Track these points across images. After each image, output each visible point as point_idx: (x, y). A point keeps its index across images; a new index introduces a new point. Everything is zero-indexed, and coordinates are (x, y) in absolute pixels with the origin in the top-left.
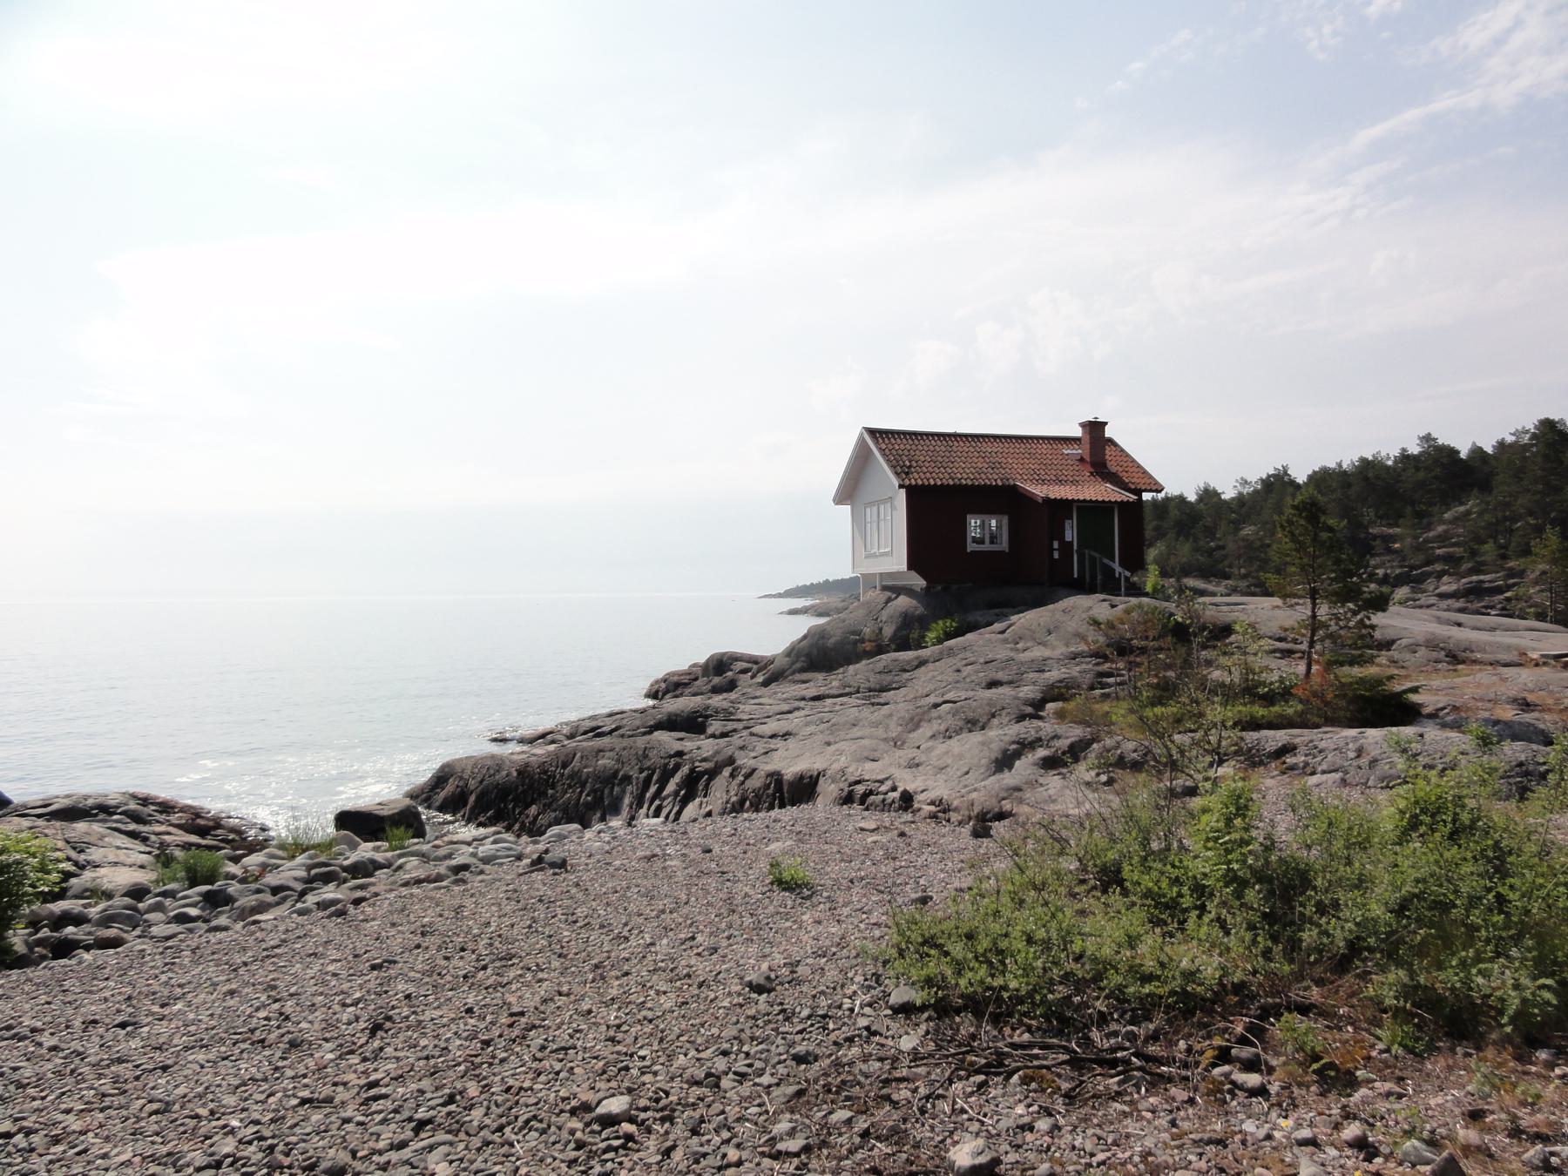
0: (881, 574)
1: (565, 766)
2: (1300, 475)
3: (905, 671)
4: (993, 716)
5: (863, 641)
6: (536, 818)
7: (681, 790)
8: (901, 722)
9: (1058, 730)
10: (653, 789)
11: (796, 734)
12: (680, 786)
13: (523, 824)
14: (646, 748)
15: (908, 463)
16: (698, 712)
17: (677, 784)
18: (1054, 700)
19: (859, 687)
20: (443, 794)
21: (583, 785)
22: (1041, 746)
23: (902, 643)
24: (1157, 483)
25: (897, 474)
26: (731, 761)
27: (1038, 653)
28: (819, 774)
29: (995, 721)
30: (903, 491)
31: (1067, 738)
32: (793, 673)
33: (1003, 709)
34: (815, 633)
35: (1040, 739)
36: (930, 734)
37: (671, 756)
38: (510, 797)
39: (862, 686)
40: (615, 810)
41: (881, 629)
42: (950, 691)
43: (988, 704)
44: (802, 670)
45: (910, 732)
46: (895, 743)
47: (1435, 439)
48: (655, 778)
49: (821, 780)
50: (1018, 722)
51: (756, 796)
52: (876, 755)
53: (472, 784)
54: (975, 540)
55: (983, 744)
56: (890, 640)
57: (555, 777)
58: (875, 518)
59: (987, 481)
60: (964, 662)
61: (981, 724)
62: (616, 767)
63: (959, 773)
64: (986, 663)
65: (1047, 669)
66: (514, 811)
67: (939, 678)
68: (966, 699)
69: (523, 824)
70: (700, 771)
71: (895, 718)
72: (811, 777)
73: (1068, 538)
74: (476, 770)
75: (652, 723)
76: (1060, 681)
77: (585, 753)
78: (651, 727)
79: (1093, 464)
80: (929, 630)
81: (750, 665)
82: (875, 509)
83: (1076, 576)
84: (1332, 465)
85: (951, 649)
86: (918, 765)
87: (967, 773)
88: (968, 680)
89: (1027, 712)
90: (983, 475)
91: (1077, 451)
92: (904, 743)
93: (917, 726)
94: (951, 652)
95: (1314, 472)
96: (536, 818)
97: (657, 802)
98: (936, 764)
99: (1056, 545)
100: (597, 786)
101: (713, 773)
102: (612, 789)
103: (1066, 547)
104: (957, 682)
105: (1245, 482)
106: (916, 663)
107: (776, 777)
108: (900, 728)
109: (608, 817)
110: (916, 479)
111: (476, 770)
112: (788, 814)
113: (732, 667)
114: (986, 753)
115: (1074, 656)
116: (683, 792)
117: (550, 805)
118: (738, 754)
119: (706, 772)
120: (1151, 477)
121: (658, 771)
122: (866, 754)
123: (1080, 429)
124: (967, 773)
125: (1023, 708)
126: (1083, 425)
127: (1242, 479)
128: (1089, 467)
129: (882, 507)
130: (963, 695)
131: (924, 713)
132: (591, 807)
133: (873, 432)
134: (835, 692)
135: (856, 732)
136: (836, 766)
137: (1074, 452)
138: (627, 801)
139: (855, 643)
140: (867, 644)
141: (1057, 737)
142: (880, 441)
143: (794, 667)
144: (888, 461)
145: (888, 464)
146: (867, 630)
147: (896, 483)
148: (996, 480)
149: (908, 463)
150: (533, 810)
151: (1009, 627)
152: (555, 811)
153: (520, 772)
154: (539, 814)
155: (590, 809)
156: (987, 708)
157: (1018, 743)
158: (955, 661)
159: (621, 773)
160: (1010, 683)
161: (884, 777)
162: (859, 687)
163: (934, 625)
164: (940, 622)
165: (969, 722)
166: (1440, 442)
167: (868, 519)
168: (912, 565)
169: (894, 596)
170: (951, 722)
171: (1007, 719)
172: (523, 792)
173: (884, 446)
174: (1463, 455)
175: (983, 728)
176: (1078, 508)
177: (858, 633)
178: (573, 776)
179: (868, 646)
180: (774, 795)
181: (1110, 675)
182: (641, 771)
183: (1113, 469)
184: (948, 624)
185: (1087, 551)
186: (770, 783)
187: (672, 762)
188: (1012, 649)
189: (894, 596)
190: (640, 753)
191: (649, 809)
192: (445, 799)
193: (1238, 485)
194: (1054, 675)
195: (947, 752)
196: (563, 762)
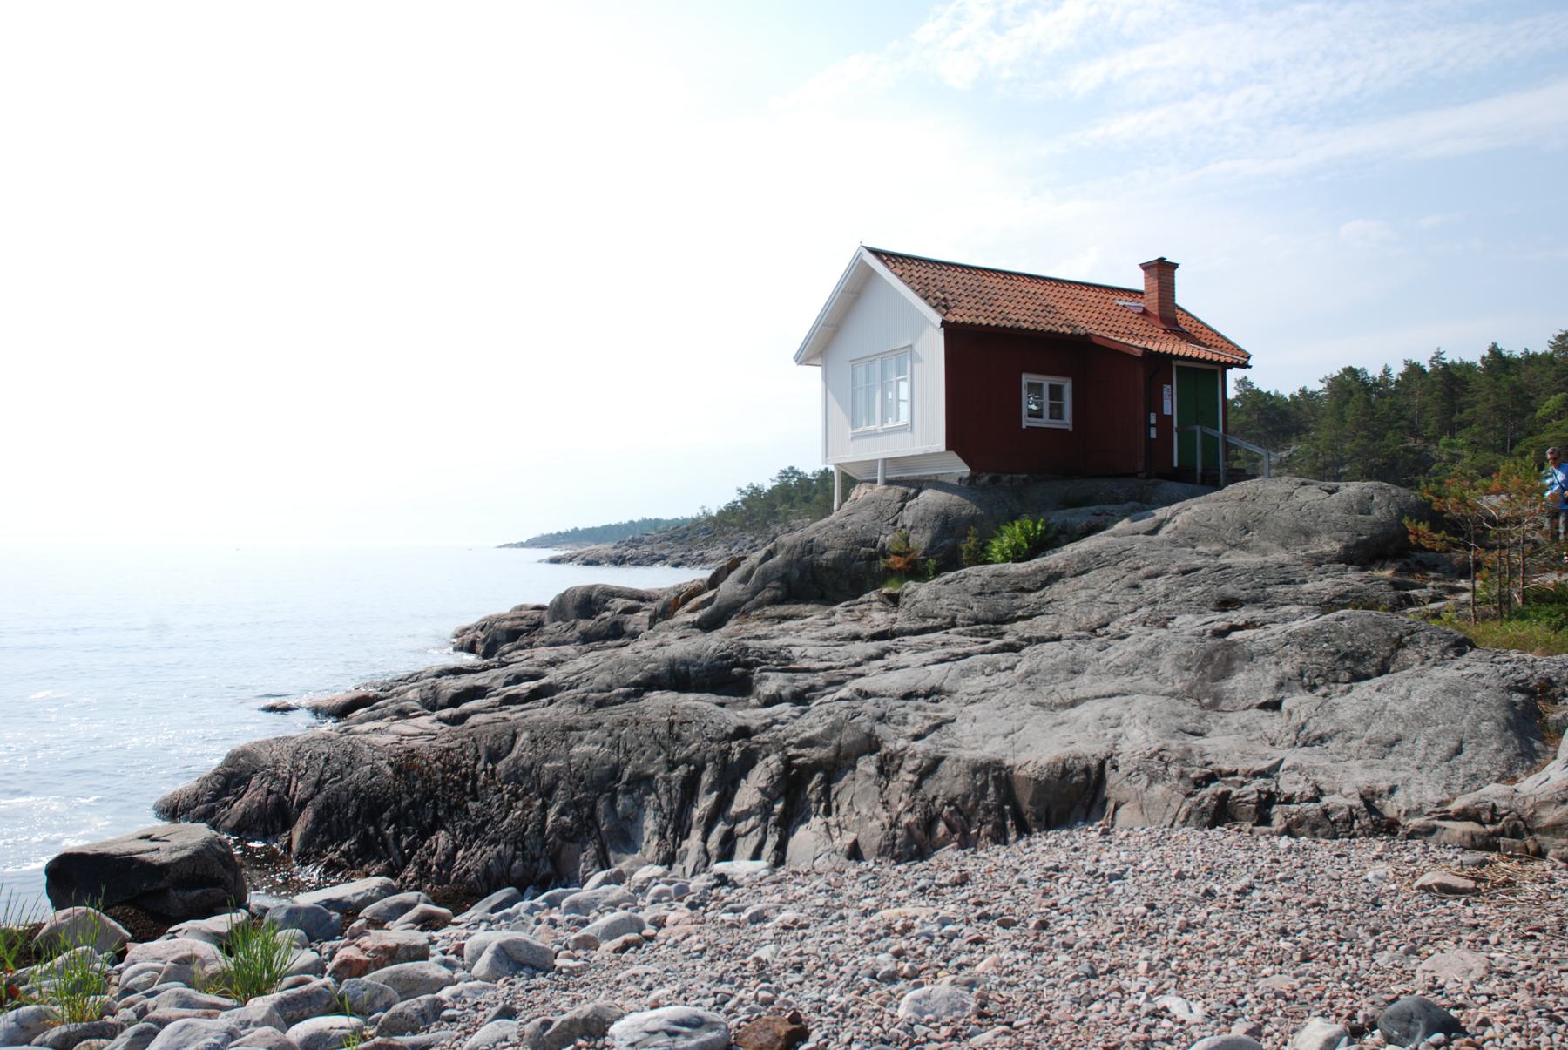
0: (885, 460)
1: (494, 756)
3: (1022, 590)
5: (884, 553)
6: (451, 857)
7: (775, 801)
8: (1184, 662)
10: (705, 803)
12: (769, 796)
13: (423, 864)
14: (671, 724)
16: (729, 656)
17: (763, 791)
20: (239, 807)
21: (548, 793)
26: (871, 744)
28: (1102, 764)
29: (1410, 654)
37: (731, 737)
38: (386, 815)
40: (626, 840)
44: (774, 601)
47: (1251, 383)
48: (706, 778)
49: (1112, 778)
51: (958, 811)
53: (300, 789)
54: (1032, 414)
56: (925, 553)
57: (475, 778)
62: (614, 758)
65: (1298, 580)
66: (397, 840)
69: (423, 864)
70: (805, 765)
72: (1087, 770)
73: (1167, 411)
74: (303, 763)
75: (637, 677)
77: (538, 733)
78: (636, 684)
83: (1176, 464)
91: (1137, 305)
96: (451, 857)
97: (720, 828)
100: (579, 795)
101: (836, 767)
102: (612, 802)
103: (1165, 421)
106: (1040, 578)
107: (996, 775)
109: (612, 855)
111: (303, 763)
112: (1047, 847)
116: (778, 807)
117: (479, 830)
118: (880, 730)
119: (817, 766)
121: (710, 766)
123: (1142, 272)
126: (1146, 267)
128: (1157, 322)
132: (574, 836)
138: (650, 823)
139: (873, 558)
143: (758, 597)
150: (441, 839)
152: (494, 842)
153: (398, 770)
154: (456, 848)
155: (571, 840)
159: (628, 771)
162: (954, 618)
165: (1345, 657)
166: (1255, 386)
168: (953, 442)
169: (912, 491)
172: (412, 805)
174: (1428, 369)
175: (1383, 670)
176: (1178, 368)
178: (516, 775)
179: (896, 562)
180: (1000, 808)
182: (672, 765)
183: (1187, 329)
185: (1198, 428)
186: (985, 786)
187: (736, 749)
189: (912, 491)
190: (662, 731)
191: (705, 840)
192: (244, 815)
196: (489, 749)
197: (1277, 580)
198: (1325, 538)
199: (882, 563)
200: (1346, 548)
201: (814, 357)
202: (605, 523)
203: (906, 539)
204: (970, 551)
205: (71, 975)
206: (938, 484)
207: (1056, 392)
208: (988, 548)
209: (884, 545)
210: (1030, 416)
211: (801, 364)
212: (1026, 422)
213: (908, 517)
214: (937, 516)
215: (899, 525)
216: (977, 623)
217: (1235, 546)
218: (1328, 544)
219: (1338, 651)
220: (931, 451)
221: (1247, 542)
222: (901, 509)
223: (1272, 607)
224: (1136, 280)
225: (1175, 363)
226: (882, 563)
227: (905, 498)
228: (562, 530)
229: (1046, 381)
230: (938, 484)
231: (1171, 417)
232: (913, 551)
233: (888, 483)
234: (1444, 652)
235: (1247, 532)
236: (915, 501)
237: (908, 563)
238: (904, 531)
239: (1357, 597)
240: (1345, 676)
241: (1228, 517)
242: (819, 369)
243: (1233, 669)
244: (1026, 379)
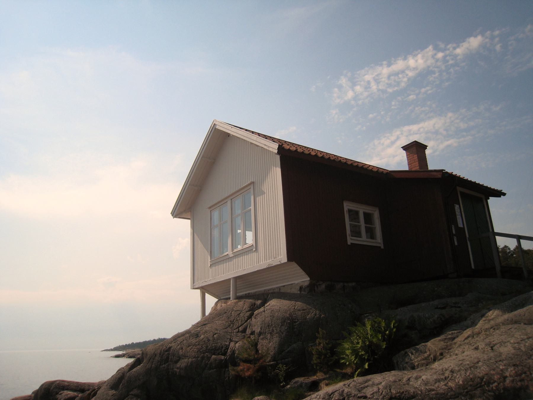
0: (236, 279)
2: (130, 343)
5: (234, 361)
56: (274, 359)
81: (76, 394)
83: (473, 267)
123: (404, 153)
139: (223, 366)
140: (242, 366)
169: (259, 302)
189: (259, 302)
199: (232, 371)
201: (185, 211)
202: (144, 340)
203: (255, 345)
204: (320, 354)
206: (280, 294)
207: (368, 218)
208: (338, 349)
209: (233, 352)
211: (175, 217)
213: (256, 324)
214: (284, 320)
215: (248, 331)
220: (274, 264)
222: (250, 317)
226: (232, 371)
227: (253, 308)
228: (128, 344)
229: (362, 209)
230: (280, 294)
232: (262, 358)
233: (239, 298)
236: (262, 309)
237: (258, 371)
238: (252, 337)
242: (188, 222)
244: (347, 206)
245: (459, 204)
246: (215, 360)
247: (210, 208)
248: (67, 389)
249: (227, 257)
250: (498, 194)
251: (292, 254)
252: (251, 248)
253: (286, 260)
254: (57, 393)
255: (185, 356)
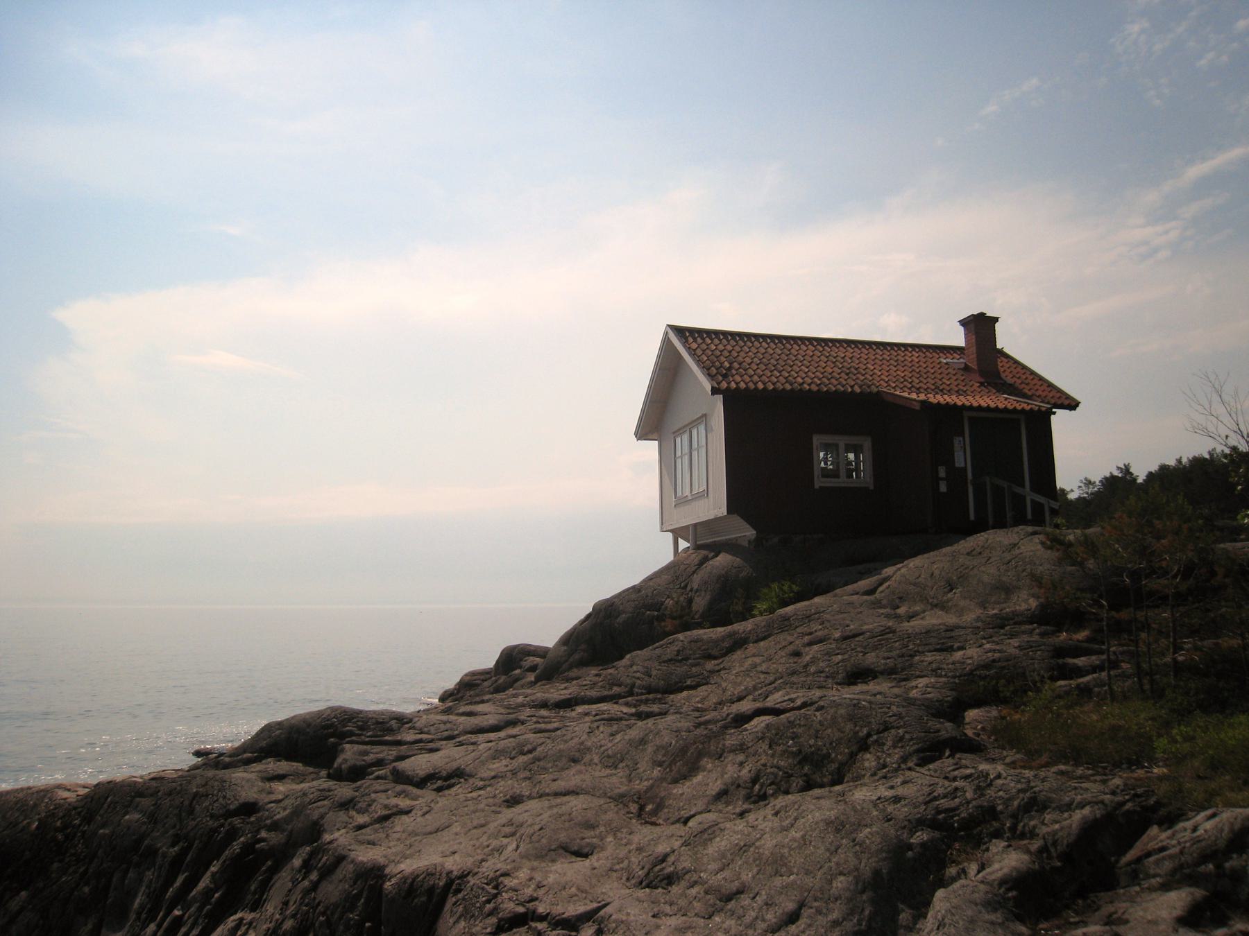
0: (695, 525)
4: (864, 746)
9: (1038, 786)
11: (471, 776)
15: (727, 365)
16: (332, 725)
18: (977, 704)
19: (633, 686)
22: (997, 835)
23: (717, 617)
24: (1068, 397)
25: (711, 376)
27: (933, 619)
29: (869, 760)
30: (719, 399)
31: (1069, 807)
32: (570, 668)
33: (887, 729)
34: (600, 610)
35: (990, 813)
36: (715, 787)
37: (230, 814)
39: (639, 682)
41: (690, 601)
42: (777, 689)
43: (851, 718)
45: (675, 781)
46: (642, 808)
50: (923, 762)
52: (590, 837)
54: (826, 473)
55: (836, 826)
58: (686, 450)
59: (839, 387)
60: (806, 639)
61: (834, 766)
63: (771, 917)
64: (845, 638)
65: (956, 645)
67: (764, 667)
68: (804, 705)
70: (262, 850)
71: (650, 749)
72: (431, 890)
73: (959, 461)
76: (986, 666)
78: (261, 750)
79: (982, 372)
80: (758, 599)
82: (686, 437)
83: (972, 517)
84: (1172, 462)
85: (786, 618)
86: (670, 880)
87: (793, 918)
88: (813, 669)
89: (944, 734)
90: (833, 380)
92: (660, 807)
93: (692, 769)
94: (786, 624)
95: (1163, 468)
98: (714, 880)
99: (942, 472)
103: (957, 476)
104: (794, 673)
105: (1089, 483)
108: (656, 772)
110: (738, 382)
113: (523, 663)
114: (846, 856)
115: (1001, 623)
120: (1059, 391)
122: (563, 837)
123: (962, 329)
124: (793, 918)
125: (933, 724)
126: (964, 323)
127: (1086, 479)
129: (694, 432)
130: (800, 696)
131: (709, 738)
133: (680, 331)
134: (594, 693)
135: (573, 777)
136: (488, 869)
137: (955, 361)
141: (1035, 805)
142: (691, 340)
143: (571, 660)
144: (699, 362)
145: (698, 365)
146: (669, 602)
147: (707, 386)
148: (852, 387)
149: (727, 365)
151: (881, 584)
156: (849, 727)
157: (933, 824)
158: (790, 639)
160: (890, 672)
161: (581, 909)
162: (633, 686)
163: (765, 590)
164: (775, 586)
167: (679, 453)
170: (764, 757)
171: (897, 755)
173: (694, 346)
175: (838, 781)
176: (970, 419)
177: (657, 606)
181: (1077, 651)
183: (1009, 380)
184: (786, 588)
186: (359, 896)
188: (888, 616)
193: (1082, 485)
194: (972, 654)
195: (747, 846)
197: (931, 647)
198: (1024, 594)
200: (1043, 607)
201: (646, 434)
205: (1171, 837)
210: (824, 476)
212: (818, 483)
215: (689, 588)
216: (649, 693)
217: (936, 606)
218: (1026, 601)
219: (800, 751)
221: (948, 601)
223: (905, 680)
224: (957, 338)
225: (966, 414)
231: (965, 469)
234: (904, 759)
235: (951, 590)
239: (1003, 668)
240: (797, 782)
241: (937, 573)
243: (698, 768)
244: (817, 440)
245: (962, 434)
246: (648, 616)
247: (674, 433)
248: (534, 656)
249: (686, 499)
250: (1072, 405)
251: (734, 503)
252: (702, 494)
253: (726, 514)
254: (521, 660)
255: (624, 612)
